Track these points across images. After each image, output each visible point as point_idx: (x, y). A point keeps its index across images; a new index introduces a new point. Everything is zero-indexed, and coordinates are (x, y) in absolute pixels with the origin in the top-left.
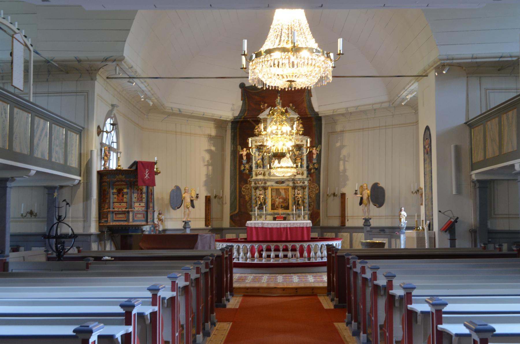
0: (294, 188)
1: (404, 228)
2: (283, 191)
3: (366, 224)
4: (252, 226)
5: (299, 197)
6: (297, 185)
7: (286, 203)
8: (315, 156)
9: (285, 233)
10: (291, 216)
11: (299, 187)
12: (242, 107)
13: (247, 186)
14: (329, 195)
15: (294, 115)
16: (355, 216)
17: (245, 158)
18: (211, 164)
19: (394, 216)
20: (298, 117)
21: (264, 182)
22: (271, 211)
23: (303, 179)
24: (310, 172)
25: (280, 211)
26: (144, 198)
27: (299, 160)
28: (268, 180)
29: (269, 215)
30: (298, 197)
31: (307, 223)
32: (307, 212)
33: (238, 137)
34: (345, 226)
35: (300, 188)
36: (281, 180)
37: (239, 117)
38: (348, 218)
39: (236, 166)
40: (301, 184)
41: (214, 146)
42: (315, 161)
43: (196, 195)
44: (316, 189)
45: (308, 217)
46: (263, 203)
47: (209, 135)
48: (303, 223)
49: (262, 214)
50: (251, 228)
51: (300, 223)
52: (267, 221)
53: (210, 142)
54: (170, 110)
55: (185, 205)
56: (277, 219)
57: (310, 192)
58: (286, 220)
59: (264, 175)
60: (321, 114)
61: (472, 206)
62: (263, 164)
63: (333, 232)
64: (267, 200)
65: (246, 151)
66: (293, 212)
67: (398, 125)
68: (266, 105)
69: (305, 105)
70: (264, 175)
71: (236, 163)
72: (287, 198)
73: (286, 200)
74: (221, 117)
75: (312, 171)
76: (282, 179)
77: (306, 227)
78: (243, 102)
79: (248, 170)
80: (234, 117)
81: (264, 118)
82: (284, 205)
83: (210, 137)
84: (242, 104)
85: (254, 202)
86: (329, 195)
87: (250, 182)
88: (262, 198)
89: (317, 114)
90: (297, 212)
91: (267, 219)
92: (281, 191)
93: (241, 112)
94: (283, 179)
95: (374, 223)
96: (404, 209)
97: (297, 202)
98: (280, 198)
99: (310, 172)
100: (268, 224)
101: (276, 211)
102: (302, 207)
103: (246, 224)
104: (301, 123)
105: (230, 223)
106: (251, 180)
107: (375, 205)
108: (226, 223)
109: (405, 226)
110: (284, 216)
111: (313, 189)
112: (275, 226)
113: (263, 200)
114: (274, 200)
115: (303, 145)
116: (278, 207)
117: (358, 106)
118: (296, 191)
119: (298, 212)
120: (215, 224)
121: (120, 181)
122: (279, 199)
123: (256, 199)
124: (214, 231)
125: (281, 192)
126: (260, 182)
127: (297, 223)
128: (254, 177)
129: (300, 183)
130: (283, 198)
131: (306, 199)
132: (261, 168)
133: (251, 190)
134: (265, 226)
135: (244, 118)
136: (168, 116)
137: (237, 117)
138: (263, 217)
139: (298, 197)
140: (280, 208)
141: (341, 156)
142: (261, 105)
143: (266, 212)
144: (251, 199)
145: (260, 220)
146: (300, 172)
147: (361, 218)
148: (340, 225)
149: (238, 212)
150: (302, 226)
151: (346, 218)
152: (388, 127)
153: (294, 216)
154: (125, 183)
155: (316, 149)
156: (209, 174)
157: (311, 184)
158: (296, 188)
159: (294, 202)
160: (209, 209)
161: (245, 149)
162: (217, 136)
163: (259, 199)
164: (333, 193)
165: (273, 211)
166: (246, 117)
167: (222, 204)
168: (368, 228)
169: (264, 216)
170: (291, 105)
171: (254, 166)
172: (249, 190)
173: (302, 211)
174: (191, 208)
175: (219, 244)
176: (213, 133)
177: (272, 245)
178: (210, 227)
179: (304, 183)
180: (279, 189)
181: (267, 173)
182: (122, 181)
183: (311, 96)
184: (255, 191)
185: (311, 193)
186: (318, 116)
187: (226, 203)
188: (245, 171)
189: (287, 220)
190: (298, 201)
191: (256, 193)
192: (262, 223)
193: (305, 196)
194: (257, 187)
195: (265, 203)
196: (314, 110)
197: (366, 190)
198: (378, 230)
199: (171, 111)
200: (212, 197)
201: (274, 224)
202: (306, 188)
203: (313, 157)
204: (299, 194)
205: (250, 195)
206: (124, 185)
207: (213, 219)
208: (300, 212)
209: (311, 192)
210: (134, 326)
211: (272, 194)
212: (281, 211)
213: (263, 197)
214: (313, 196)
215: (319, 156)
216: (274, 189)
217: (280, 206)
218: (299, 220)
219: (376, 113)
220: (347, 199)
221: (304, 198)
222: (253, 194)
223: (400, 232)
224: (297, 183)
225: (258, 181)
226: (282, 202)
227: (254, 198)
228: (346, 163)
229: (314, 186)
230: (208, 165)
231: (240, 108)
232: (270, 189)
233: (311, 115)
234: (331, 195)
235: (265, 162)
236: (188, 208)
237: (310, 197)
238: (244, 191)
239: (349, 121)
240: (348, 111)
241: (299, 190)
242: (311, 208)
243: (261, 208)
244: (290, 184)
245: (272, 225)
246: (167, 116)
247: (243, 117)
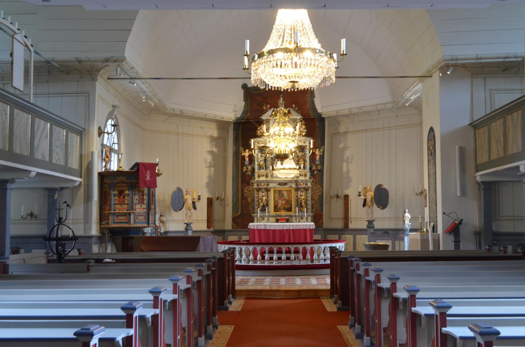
0: (297, 189)
1: (408, 230)
2: (286, 192)
3: (369, 226)
4: (254, 228)
5: (302, 199)
6: (300, 186)
7: (289, 204)
8: (318, 158)
9: (288, 235)
10: (294, 218)
11: (302, 189)
12: (244, 108)
13: (249, 188)
14: (332, 197)
15: (297, 116)
16: (359, 218)
17: (247, 159)
18: (213, 166)
19: (398, 218)
20: (301, 118)
21: (266, 184)
22: (273, 213)
23: (306, 180)
24: (313, 174)
25: (283, 213)
26: (145, 200)
27: (302, 161)
28: (270, 182)
29: (272, 217)
30: (301, 199)
31: (310, 225)
32: (309, 214)
33: (240, 138)
34: (348, 228)
35: (302, 190)
36: (284, 181)
37: (241, 118)
38: (351, 220)
39: (238, 168)
40: (304, 186)
41: (216, 147)
42: (318, 163)
43: (198, 197)
44: (319, 191)
45: (311, 218)
46: (265, 205)
47: (211, 136)
48: (306, 225)
49: (264, 216)
50: (254, 230)
51: (303, 225)
52: (269, 222)
53: (212, 143)
54: (171, 111)
55: (187, 207)
56: (279, 221)
57: (313, 194)
58: (288, 222)
59: (267, 176)
60: (324, 115)
61: (477, 208)
62: (266, 166)
63: (336, 234)
64: (269, 201)
65: (248, 152)
66: (296, 214)
67: (401, 126)
68: (269, 106)
69: (308, 106)
70: (267, 176)
71: (238, 165)
72: (290, 200)
73: (289, 202)
74: (223, 118)
75: (315, 172)
76: (284, 181)
77: (309, 229)
78: (245, 103)
79: (250, 171)
80: (236, 118)
81: (267, 119)
82: (286, 207)
83: (212, 139)
84: (245, 105)
85: (256, 203)
86: (332, 197)
87: (252, 183)
88: (264, 200)
89: (320, 115)
90: (300, 214)
91: (270, 221)
92: (283, 192)
93: (243, 113)
94: (286, 181)
95: (377, 225)
96: (408, 211)
97: (300, 204)
98: (283, 200)
99: (313, 174)
100: (270, 225)
101: (278, 213)
102: (305, 209)
103: (249, 226)
104: (304, 124)
105: (232, 225)
106: (253, 182)
107: (379, 207)
108: (228, 225)
109: (409, 228)
110: (287, 218)
111: (316, 190)
112: (278, 228)
113: (266, 202)
114: (277, 202)
115: (306, 146)
116: (281, 209)
117: (362, 107)
118: (299, 192)
119: (301, 214)
120: (217, 226)
121: (121, 183)
122: (282, 201)
123: (258, 200)
124: (217, 233)
125: (283, 194)
126: (263, 184)
127: (300, 225)
128: (257, 179)
129: (303, 184)
130: (285, 200)
131: (309, 201)
132: (263, 170)
133: (253, 192)
134: (268, 228)
135: (246, 119)
136: (169, 117)
137: (239, 118)
138: (266, 219)
139: (301, 199)
140: (283, 210)
141: (345, 158)
142: (263, 106)
143: (269, 214)
144: (253, 200)
145: (262, 222)
146: (303, 174)
147: (364, 219)
148: (343, 227)
149: (240, 214)
150: (304, 228)
151: (350, 220)
152: (392, 128)
153: (296, 218)
154: (126, 185)
155: (319, 151)
156: (211, 176)
157: (314, 186)
158: (299, 190)
159: (297, 203)
160: (211, 211)
161: (247, 151)
162: (219, 138)
163: (262, 201)
164: (336, 195)
165: (275, 213)
166: (249, 118)
167: (224, 206)
168: (372, 230)
169: (267, 218)
170: (294, 106)
171: (256, 167)
172: (252, 192)
173: (304, 213)
174: (193, 210)
175: (221, 247)
176: (215, 134)
177: (275, 247)
178: (212, 229)
179: (307, 184)
180: (281, 191)
181: (269, 175)
182: (123, 182)
183: (314, 97)
184: (257, 193)
185: (314, 195)
186: (321, 117)
187: (228, 205)
188: (247, 173)
189: (289, 221)
190: (301, 203)
191: (259, 195)
192: (265, 225)
193: (307, 197)
194: (260, 189)
195: (267, 205)
196: (317, 111)
197: (370, 192)
198: (381, 232)
199: (173, 112)
200: (214, 199)
201: (277, 226)
202: (309, 189)
203: (316, 159)
204: (302, 195)
205: (253, 196)
206: (125, 186)
207: (215, 221)
208: (303, 214)
209: (314, 193)
210: (135, 329)
211: (275, 196)
212: (283, 213)
213: (265, 199)
214: (316, 198)
215: (322, 157)
216: (276, 190)
217: (283, 208)
218: (302, 222)
219: (379, 114)
220: (351, 200)
221: (307, 200)
222: (256, 195)
223: (404, 234)
224: (300, 185)
225: (260, 183)
226: (285, 204)
227: (256, 199)
228: (350, 164)
229: (317, 187)
230: (210, 167)
231: (243, 109)
232: (272, 191)
233: (314, 116)
234: (334, 196)
235: (267, 164)
236: (190, 210)
237: (313, 198)
238: (247, 192)
239: (353, 122)
240: (351, 112)
241: (301, 192)
242: (314, 210)
243: (263, 210)
244: (292, 186)
245: (275, 227)
246: (169, 117)
247: (245, 118)
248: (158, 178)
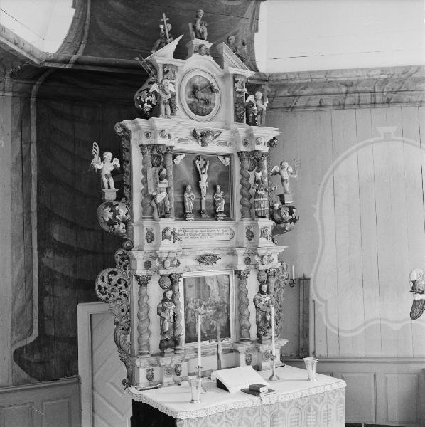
2: (215, 283)
33: (33, 120)
39: (29, 204)
61: (19, 50)
65: (111, 161)
71: (30, 194)
78: (76, 12)
92: (208, 282)
149: (38, 339)
172: (122, 285)
180: (204, 278)
211: (188, 296)
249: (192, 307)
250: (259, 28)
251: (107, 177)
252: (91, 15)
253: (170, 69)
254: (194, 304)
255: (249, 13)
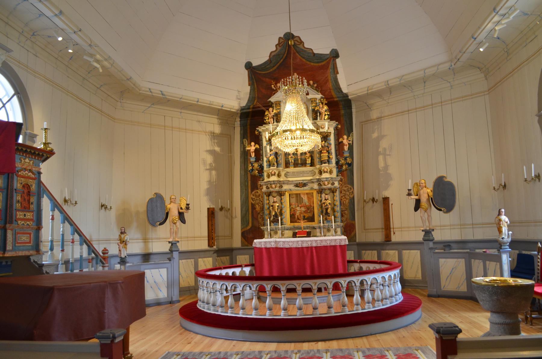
0: (320, 192)
1: (507, 243)
2: (306, 196)
3: (426, 238)
4: (262, 246)
5: (328, 204)
6: (324, 187)
7: (310, 212)
8: (346, 148)
9: (309, 253)
10: (318, 230)
11: (327, 190)
12: (250, 94)
13: (257, 192)
14: (367, 201)
15: (314, 95)
16: (404, 228)
17: (253, 155)
18: (215, 169)
19: (464, 225)
20: (322, 98)
21: (278, 185)
22: (290, 225)
23: (331, 178)
24: (340, 170)
25: (303, 224)
26: (32, 203)
27: (325, 153)
28: (284, 183)
29: (287, 230)
30: (326, 204)
31: (341, 240)
32: (339, 223)
34: (391, 241)
35: (328, 192)
36: (302, 181)
37: (247, 107)
38: (394, 230)
40: (330, 186)
41: (218, 146)
42: (346, 154)
44: (350, 193)
45: (341, 230)
46: (278, 213)
47: (211, 132)
48: (336, 240)
49: (277, 230)
50: (261, 249)
51: (331, 240)
52: (285, 238)
53: (213, 141)
54: (147, 91)
55: (171, 219)
56: (297, 236)
57: (342, 197)
58: (310, 237)
59: (279, 176)
60: (351, 95)
62: (277, 162)
63: (375, 250)
64: (284, 209)
65: (255, 146)
66: (320, 225)
69: (330, 85)
70: (279, 176)
72: (311, 206)
73: (310, 209)
74: (222, 106)
75: (344, 167)
76: (303, 180)
77: (340, 246)
78: (251, 88)
79: (257, 170)
80: (240, 107)
81: (276, 101)
82: (307, 215)
83: (213, 135)
84: (250, 90)
85: (267, 212)
86: (367, 201)
87: (261, 186)
88: (277, 207)
89: (346, 95)
90: (325, 224)
91: (285, 236)
92: (302, 196)
93: (249, 100)
94: (305, 180)
95: (437, 236)
96: (505, 212)
97: (325, 211)
98: (302, 207)
99: (340, 170)
100: (284, 242)
101: (296, 224)
102: (333, 217)
103: (254, 243)
104: (326, 104)
105: (241, 241)
106: (262, 184)
107: (440, 210)
108: (237, 242)
109: (510, 240)
110: (308, 230)
111: (346, 192)
112: (294, 246)
113: (279, 210)
115: (330, 133)
116: (300, 219)
117: (403, 76)
118: (323, 195)
119: (327, 224)
120: (223, 244)
122: (300, 207)
123: (269, 208)
124: (221, 252)
125: (302, 198)
126: (273, 186)
127: (326, 241)
128: (266, 180)
129: (328, 184)
130: (305, 206)
131: (338, 207)
132: (274, 166)
133: (262, 197)
134: (281, 246)
135: (253, 108)
136: (151, 105)
137: (244, 107)
138: (279, 232)
139: (326, 204)
140: (302, 219)
141: (381, 150)
142: (271, 85)
143: (283, 226)
144: (262, 209)
145: (274, 237)
146: (327, 169)
147: (419, 229)
148: (384, 241)
150: (333, 244)
151: (392, 230)
152: (444, 103)
153: (321, 230)
155: (347, 139)
156: (212, 181)
157: (343, 186)
158: (322, 192)
159: (321, 210)
160: (212, 225)
161: (253, 144)
162: (221, 135)
163: (273, 208)
164: (372, 198)
165: (292, 224)
166: (256, 106)
167: (231, 218)
168: (431, 244)
169: (280, 231)
171: (265, 164)
172: (260, 197)
173: (332, 223)
174: (179, 223)
175: (203, 281)
176: (217, 129)
177: (282, 284)
178: (215, 247)
180: (300, 194)
181: (283, 174)
183: (338, 73)
184: (267, 198)
186: (347, 98)
187: (236, 217)
188: (254, 172)
189: (311, 235)
190: (327, 209)
191: (269, 201)
192: (276, 242)
193: (335, 201)
194: (270, 192)
195: (281, 214)
196: (342, 92)
197: (425, 188)
198: (441, 246)
199: (150, 94)
200: (217, 210)
201: (293, 242)
202: (336, 190)
203: (343, 149)
204: (328, 199)
205: (262, 203)
207: (219, 237)
208: (330, 224)
209: (344, 196)
211: (291, 202)
212: (303, 224)
213: (278, 206)
214: (346, 202)
215: (351, 147)
216: (293, 194)
217: (302, 218)
218: (329, 236)
219: (425, 87)
220: (392, 204)
221: (335, 205)
222: (266, 202)
223: (501, 250)
224: (325, 185)
225: (271, 184)
226: (305, 212)
227: (266, 207)
228: (388, 157)
229: (347, 188)
230: (210, 170)
231: (248, 96)
232: (287, 195)
233: (338, 97)
234: (369, 200)
235: (279, 159)
236: (175, 223)
238: (254, 199)
239: (388, 103)
240: (388, 84)
241: (326, 195)
242: (344, 219)
243: (275, 221)
244: (314, 186)
245: (291, 244)
246: (151, 104)
247: (251, 106)
248: (254, 65)
249: (293, 207)
250: (339, 71)
251: (252, 153)
252: (257, 86)
253: (313, 100)
254: (295, 206)
255: (331, 66)
